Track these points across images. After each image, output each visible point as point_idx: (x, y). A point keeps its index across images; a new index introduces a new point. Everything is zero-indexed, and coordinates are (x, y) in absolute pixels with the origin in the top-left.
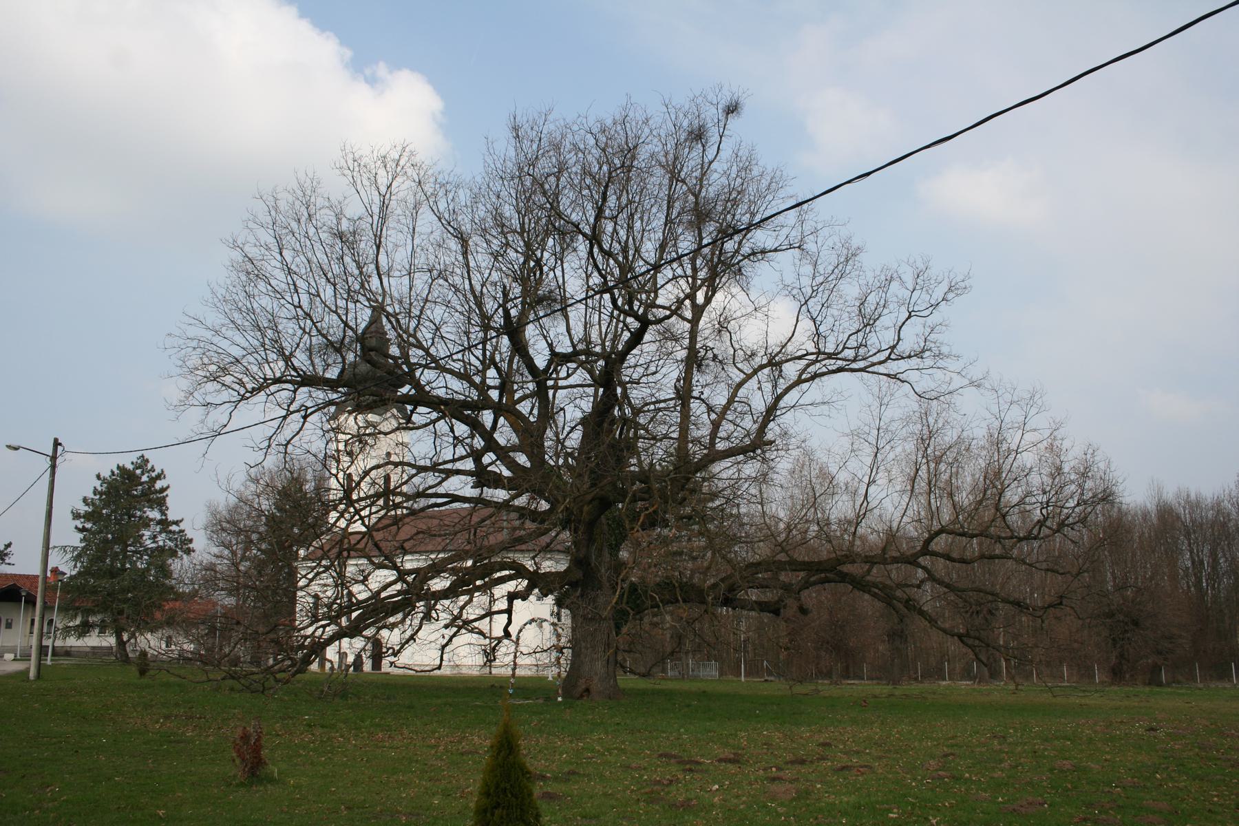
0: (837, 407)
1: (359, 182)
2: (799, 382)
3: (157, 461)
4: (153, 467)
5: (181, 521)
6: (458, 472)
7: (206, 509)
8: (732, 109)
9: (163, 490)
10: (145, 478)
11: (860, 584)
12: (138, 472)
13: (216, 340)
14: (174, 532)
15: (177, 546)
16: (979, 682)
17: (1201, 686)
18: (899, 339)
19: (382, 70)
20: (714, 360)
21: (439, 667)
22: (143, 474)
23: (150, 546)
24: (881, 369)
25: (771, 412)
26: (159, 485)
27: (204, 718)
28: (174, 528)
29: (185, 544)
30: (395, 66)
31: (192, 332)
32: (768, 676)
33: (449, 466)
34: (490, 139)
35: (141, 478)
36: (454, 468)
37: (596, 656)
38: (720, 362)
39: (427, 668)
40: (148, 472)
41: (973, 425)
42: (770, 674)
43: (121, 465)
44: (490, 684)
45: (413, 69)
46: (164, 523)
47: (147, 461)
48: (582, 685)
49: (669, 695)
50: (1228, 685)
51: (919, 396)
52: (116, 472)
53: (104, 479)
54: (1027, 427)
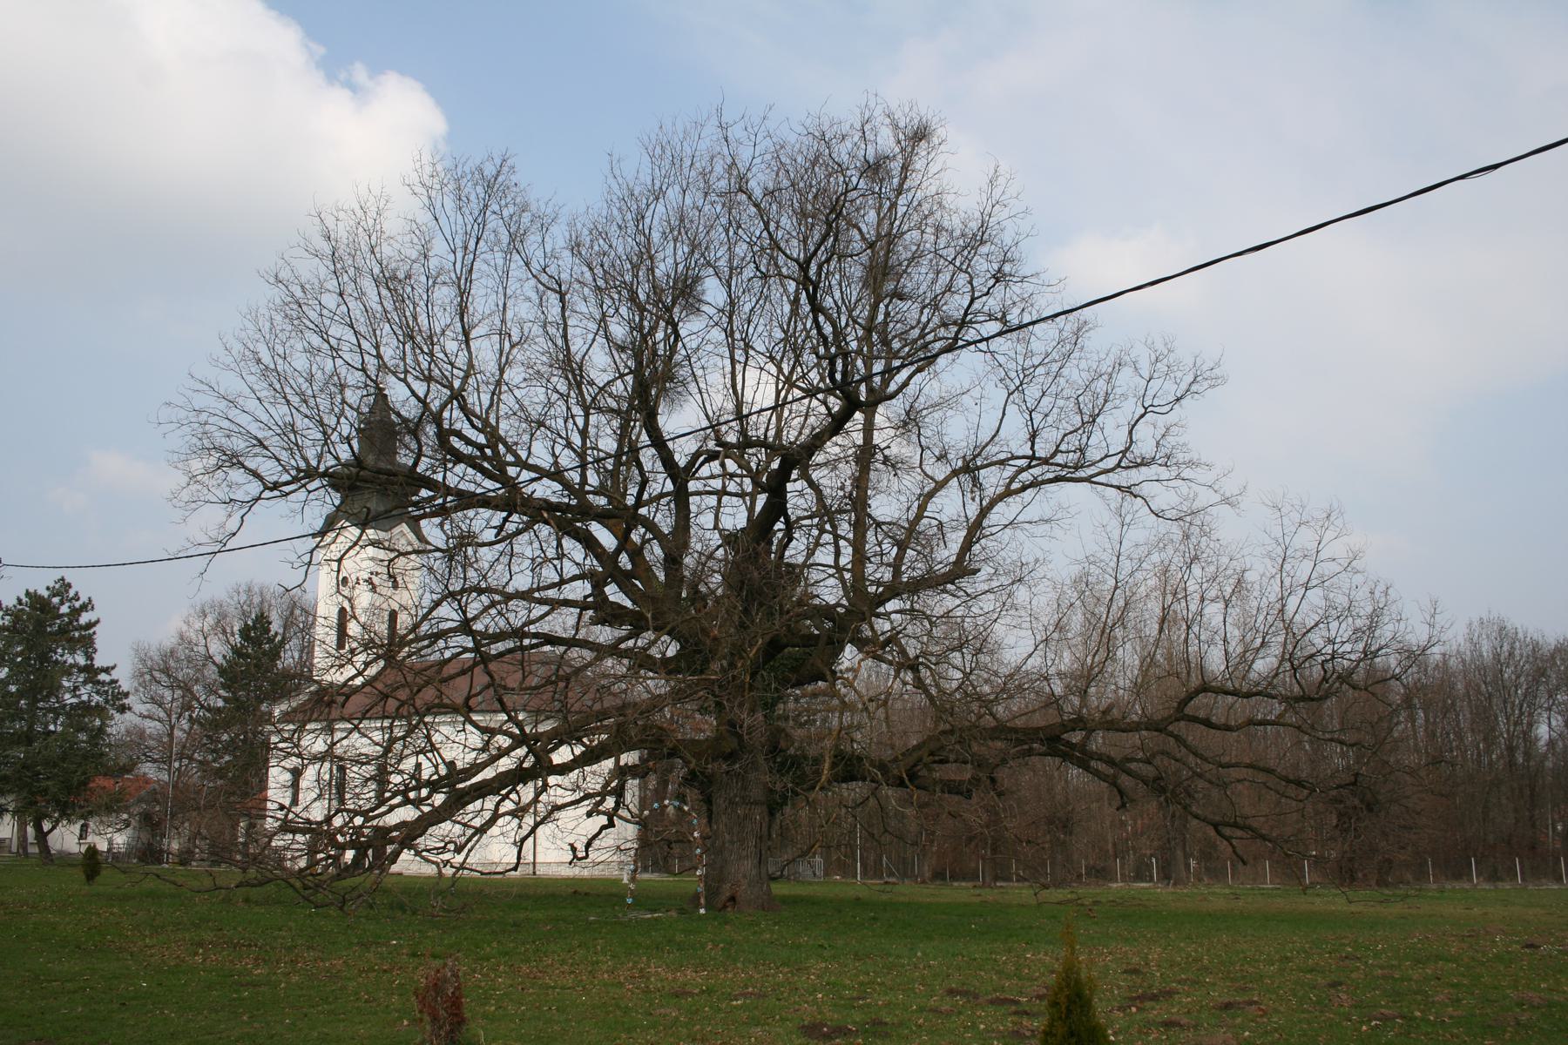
0: (1065, 527)
1: (438, 206)
2: (1008, 493)
3: (82, 586)
4: (77, 594)
5: (113, 668)
6: (567, 603)
7: (133, 653)
8: (920, 135)
9: (90, 625)
10: (64, 609)
11: (1083, 758)
12: (56, 600)
13: (233, 413)
14: (103, 683)
15: (107, 701)
16: (1175, 884)
17: (1434, 886)
18: (1132, 442)
19: (360, 74)
20: (884, 463)
21: (515, 869)
22: (62, 603)
23: (68, 702)
24: (1113, 478)
25: (975, 530)
26: (84, 618)
27: (256, 945)
28: (103, 677)
29: (119, 699)
30: (376, 70)
31: (201, 401)
32: (888, 876)
33: (552, 593)
34: (615, 157)
35: (59, 609)
36: (562, 597)
37: (744, 853)
38: (893, 466)
39: (499, 869)
40: (70, 601)
41: (1245, 552)
42: (891, 874)
43: (32, 590)
44: (570, 891)
45: (403, 72)
46: (91, 671)
47: (69, 586)
48: (726, 891)
49: (810, 901)
50: (1467, 886)
51: (1157, 515)
52: (25, 599)
53: (7, 609)
54: (1322, 556)
